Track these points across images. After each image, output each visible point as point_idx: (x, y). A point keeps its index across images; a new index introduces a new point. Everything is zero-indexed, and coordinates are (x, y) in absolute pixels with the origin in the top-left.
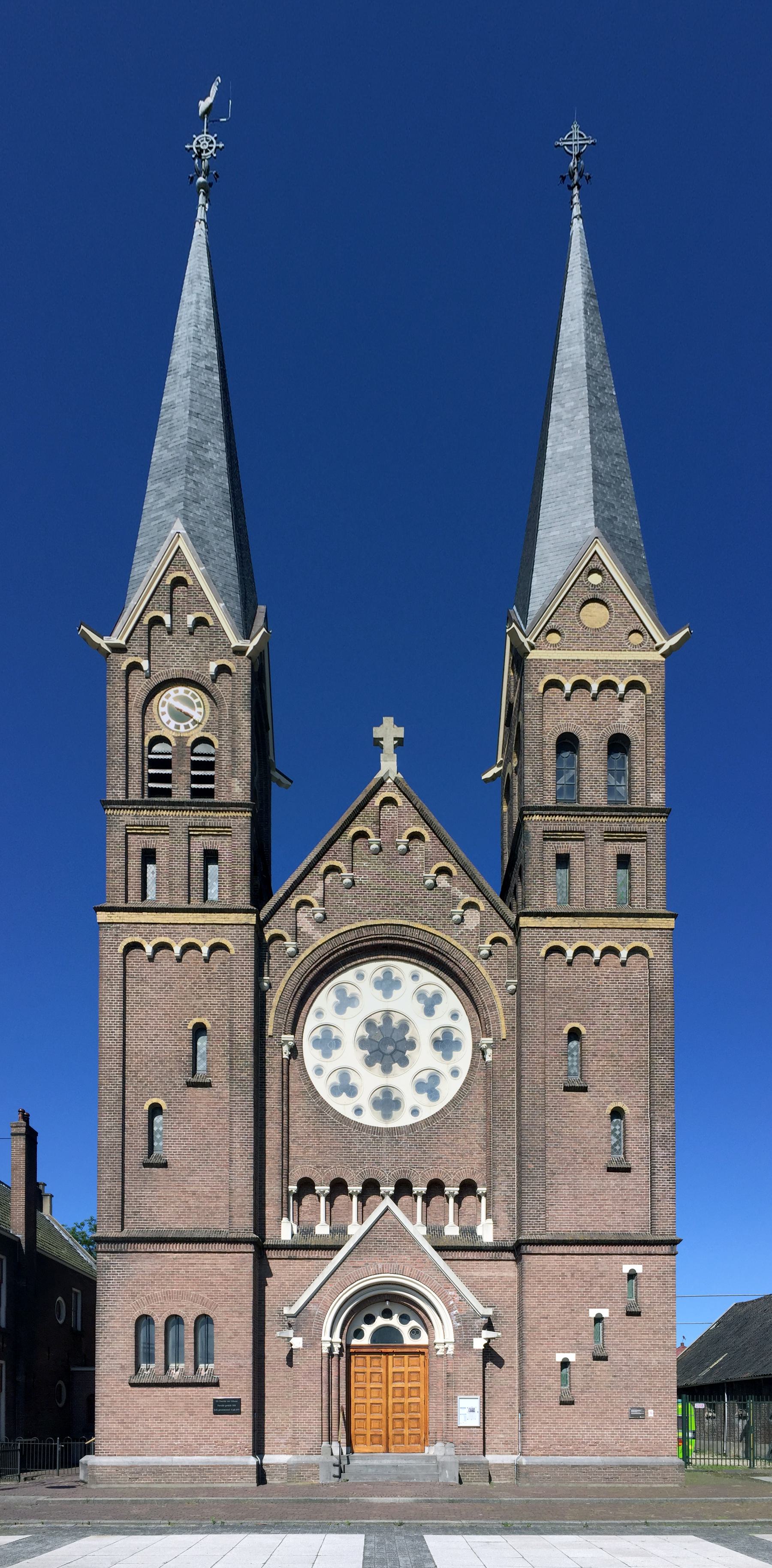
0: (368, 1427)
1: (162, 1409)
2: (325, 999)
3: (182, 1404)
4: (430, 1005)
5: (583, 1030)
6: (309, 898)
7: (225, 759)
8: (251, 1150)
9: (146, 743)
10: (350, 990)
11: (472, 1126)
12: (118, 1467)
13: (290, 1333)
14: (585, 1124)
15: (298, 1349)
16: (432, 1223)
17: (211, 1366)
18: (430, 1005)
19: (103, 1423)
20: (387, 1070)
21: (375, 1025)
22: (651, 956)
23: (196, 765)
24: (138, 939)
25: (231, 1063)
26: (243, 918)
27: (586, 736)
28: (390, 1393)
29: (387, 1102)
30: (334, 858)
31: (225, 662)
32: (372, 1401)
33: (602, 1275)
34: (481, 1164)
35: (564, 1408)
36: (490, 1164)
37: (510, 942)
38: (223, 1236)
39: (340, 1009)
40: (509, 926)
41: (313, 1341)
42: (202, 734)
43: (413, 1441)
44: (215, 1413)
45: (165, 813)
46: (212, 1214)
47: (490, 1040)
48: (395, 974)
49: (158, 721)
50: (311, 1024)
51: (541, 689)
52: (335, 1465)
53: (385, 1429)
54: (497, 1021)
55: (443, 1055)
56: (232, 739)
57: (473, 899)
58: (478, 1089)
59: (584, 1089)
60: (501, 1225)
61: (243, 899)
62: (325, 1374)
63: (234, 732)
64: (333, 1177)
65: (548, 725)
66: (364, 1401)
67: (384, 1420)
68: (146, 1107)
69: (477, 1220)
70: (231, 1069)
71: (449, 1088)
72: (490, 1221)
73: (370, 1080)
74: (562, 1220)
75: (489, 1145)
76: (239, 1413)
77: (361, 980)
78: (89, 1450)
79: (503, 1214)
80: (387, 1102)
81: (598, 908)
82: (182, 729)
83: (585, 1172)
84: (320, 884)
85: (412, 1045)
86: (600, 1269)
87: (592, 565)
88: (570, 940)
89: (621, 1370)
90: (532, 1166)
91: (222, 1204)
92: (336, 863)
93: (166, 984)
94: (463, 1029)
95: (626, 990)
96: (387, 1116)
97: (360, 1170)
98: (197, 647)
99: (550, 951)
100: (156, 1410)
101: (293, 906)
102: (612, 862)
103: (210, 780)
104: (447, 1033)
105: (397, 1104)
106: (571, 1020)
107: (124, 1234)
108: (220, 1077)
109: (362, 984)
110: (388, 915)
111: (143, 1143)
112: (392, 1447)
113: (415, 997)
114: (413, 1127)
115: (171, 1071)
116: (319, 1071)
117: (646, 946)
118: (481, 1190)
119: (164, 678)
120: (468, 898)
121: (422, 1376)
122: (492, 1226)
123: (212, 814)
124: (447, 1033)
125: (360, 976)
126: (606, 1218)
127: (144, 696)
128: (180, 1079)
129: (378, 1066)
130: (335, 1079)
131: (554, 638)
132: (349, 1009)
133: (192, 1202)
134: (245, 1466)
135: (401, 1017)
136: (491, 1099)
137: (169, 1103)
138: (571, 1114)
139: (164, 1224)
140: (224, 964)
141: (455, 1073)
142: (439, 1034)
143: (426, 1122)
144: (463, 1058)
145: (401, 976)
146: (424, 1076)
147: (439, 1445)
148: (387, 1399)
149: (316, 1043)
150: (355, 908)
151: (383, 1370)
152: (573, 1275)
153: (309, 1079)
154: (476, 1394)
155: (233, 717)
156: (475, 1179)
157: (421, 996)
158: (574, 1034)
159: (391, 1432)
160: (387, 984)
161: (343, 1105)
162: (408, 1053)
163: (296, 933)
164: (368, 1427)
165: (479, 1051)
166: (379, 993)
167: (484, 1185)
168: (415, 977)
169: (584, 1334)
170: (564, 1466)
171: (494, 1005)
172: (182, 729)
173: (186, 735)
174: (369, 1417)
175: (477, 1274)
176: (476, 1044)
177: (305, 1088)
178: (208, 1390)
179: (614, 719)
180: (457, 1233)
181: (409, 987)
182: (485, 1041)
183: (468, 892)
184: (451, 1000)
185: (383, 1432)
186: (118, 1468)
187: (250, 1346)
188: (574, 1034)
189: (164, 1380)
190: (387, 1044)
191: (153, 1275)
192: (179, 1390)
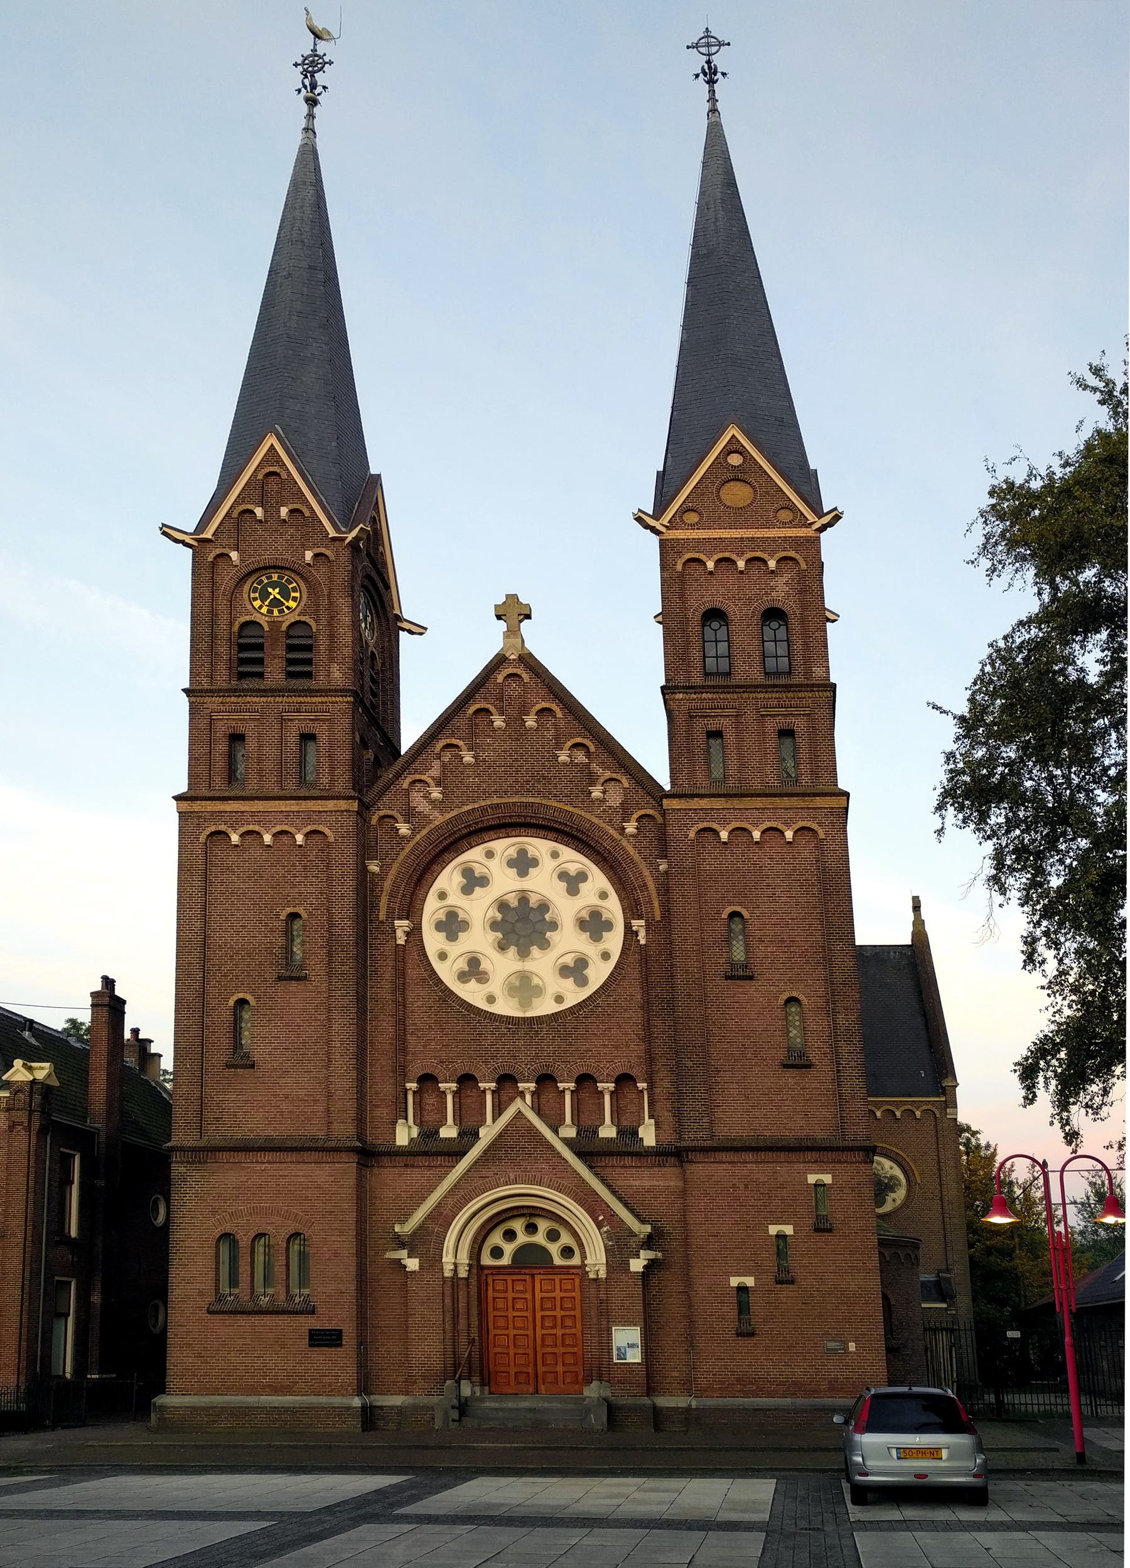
0: (512, 1363)
1: (248, 1341)
2: (449, 879)
3: (271, 1336)
4: (573, 883)
6: (423, 777)
7: (323, 643)
8: (353, 1048)
9: (236, 628)
12: (193, 1407)
13: (403, 1254)
14: (753, 1016)
15: (414, 1272)
16: (586, 1121)
17: (306, 1291)
18: (573, 883)
19: (178, 1358)
20: (524, 954)
22: (822, 836)
23: (291, 648)
24: (222, 828)
25: (329, 954)
26: (343, 805)
27: (733, 610)
28: (539, 1323)
29: (524, 987)
30: (452, 735)
31: (323, 550)
32: (516, 1332)
33: (782, 1187)
35: (742, 1341)
36: (650, 1059)
38: (320, 1144)
39: (467, 890)
41: (432, 1261)
42: (298, 618)
43: (568, 1380)
44: (311, 1345)
45: (254, 699)
46: (309, 1119)
47: (642, 922)
49: (249, 607)
50: (432, 909)
51: (679, 567)
52: (453, 1407)
53: (532, 1365)
54: (650, 902)
56: (330, 624)
57: (614, 776)
58: (634, 973)
60: (665, 1127)
61: (343, 784)
62: (448, 1301)
63: (332, 618)
65: (693, 602)
66: (506, 1332)
67: (532, 1355)
68: (231, 1003)
69: (641, 1121)
70: (330, 962)
71: (599, 973)
72: (653, 1121)
74: (734, 1123)
75: (648, 1037)
76: (340, 1345)
77: (493, 858)
78: (162, 1389)
80: (524, 987)
81: (756, 785)
82: (276, 613)
83: (756, 1069)
84: (436, 764)
85: (554, 926)
86: (781, 1179)
87: (730, 447)
88: (724, 822)
89: (812, 1296)
91: (321, 1108)
92: (454, 741)
93: (255, 873)
94: (613, 908)
95: (795, 870)
97: (492, 1064)
98: (292, 536)
100: (240, 1342)
101: (405, 785)
102: (772, 741)
103: (309, 662)
104: (595, 914)
106: (730, 903)
107: (202, 1143)
108: (316, 968)
111: (226, 1041)
112: (542, 1388)
113: (555, 876)
114: (555, 1016)
115: (261, 963)
116: (443, 956)
117: (815, 826)
119: (256, 566)
120: (608, 774)
121: (578, 1301)
122: (653, 1128)
123: (308, 699)
124: (595, 914)
125: (490, 854)
126: (785, 1121)
127: (232, 583)
128: (270, 974)
129: (513, 950)
130: (462, 965)
131: (692, 518)
132: (477, 889)
133: (284, 1106)
134: (349, 1408)
135: (539, 897)
136: (646, 984)
137: (258, 999)
138: (737, 1005)
139: (251, 1131)
140: (322, 851)
141: (606, 956)
143: (571, 1010)
144: (614, 942)
145: (538, 854)
147: (595, 1384)
148: (535, 1329)
149: (440, 926)
150: (479, 786)
151: (528, 1296)
152: (746, 1186)
153: (430, 965)
154: (635, 1325)
155: (331, 603)
156: (634, 1073)
157: (563, 876)
159: (541, 1369)
160: (523, 864)
161: (472, 993)
162: (548, 934)
163: (409, 814)
164: (512, 1363)
165: (630, 933)
166: (513, 872)
167: (645, 1081)
168: (555, 855)
169: (765, 1255)
170: (744, 1409)
171: (645, 885)
172: (276, 613)
173: (280, 619)
174: (512, 1352)
175: (637, 1183)
176: (628, 927)
177: (425, 975)
178: (302, 1319)
179: (766, 593)
180: (614, 1135)
181: (548, 865)
182: (638, 924)
183: (608, 768)
184: (598, 880)
185: (530, 1370)
186: (194, 1409)
187: (353, 1269)
189: (250, 1306)
190: (523, 924)
191: (237, 1188)
192: (268, 1320)
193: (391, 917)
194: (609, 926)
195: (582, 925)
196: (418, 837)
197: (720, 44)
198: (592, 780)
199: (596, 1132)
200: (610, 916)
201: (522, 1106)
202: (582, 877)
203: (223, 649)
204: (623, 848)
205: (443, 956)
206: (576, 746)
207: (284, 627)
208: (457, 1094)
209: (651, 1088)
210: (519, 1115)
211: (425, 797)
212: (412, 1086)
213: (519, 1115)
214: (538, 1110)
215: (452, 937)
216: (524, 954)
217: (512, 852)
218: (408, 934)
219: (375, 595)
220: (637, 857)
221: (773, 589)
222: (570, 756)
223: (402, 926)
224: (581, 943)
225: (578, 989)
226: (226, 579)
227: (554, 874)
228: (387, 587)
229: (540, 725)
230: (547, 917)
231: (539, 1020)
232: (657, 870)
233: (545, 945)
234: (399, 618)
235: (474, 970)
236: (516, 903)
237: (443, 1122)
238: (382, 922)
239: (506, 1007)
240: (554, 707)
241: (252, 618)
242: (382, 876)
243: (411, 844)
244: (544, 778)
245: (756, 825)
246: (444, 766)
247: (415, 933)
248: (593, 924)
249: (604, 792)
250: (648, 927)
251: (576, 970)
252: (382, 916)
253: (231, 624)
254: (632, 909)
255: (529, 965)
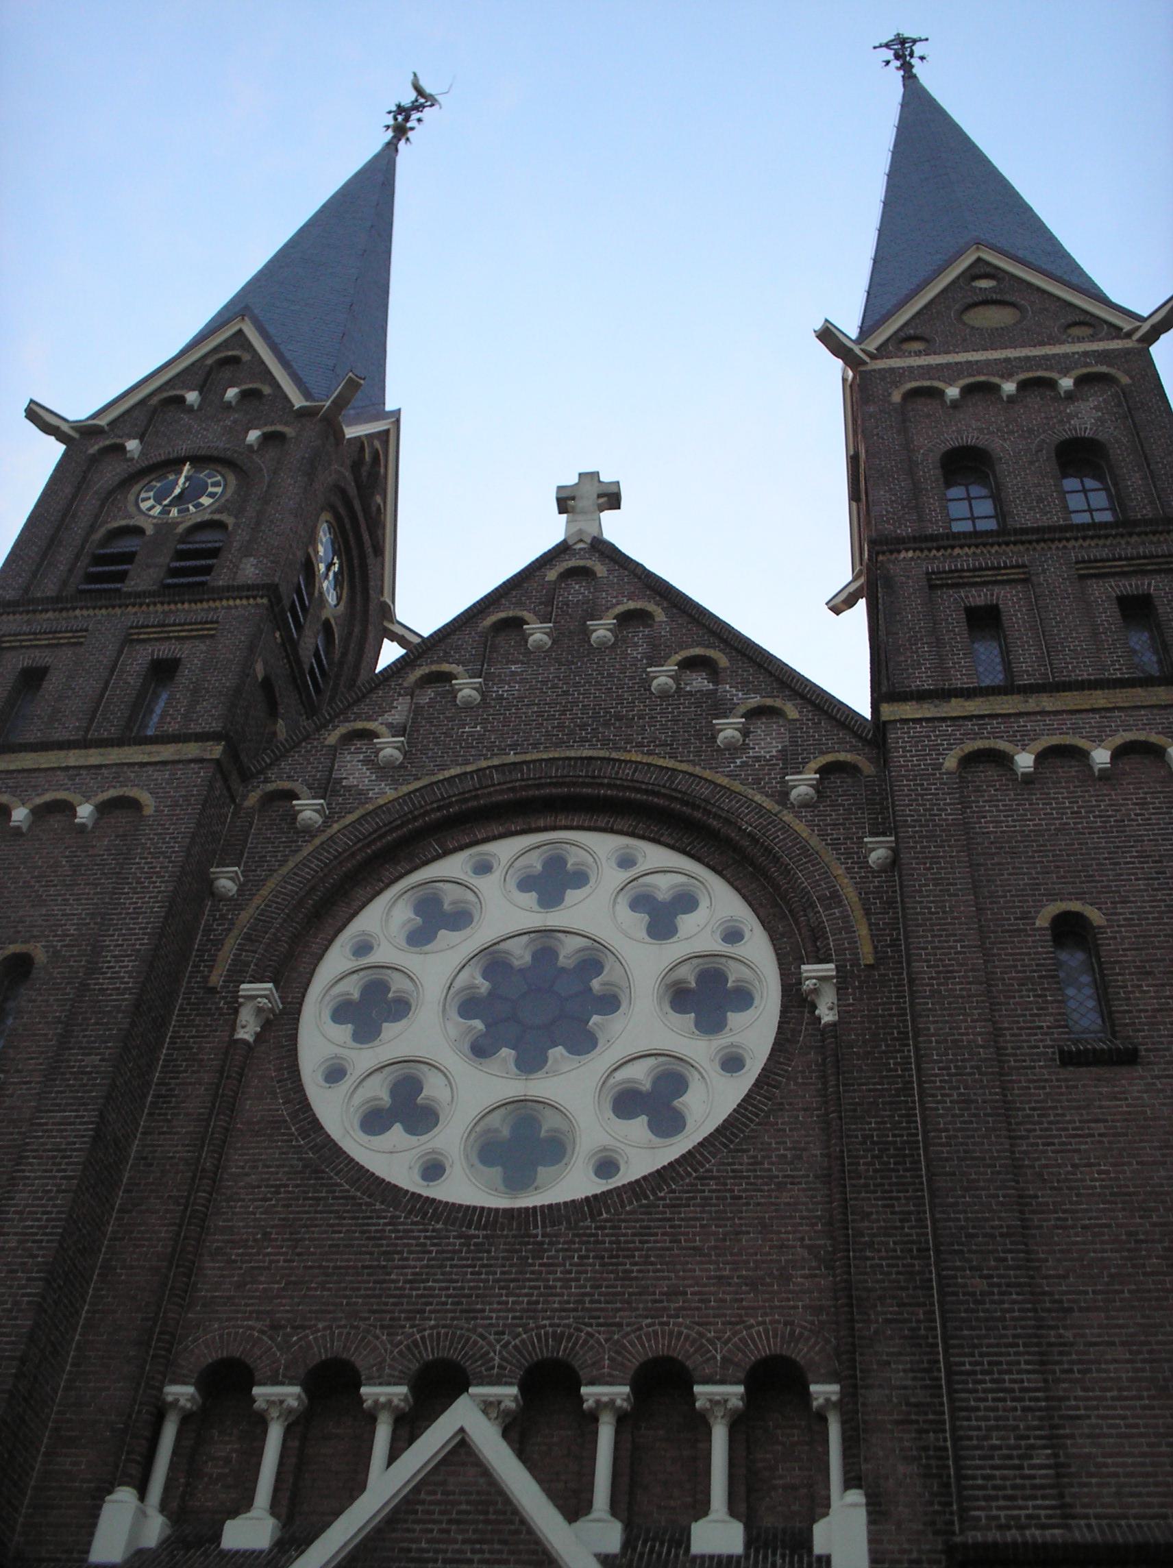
2: (384, 918)
4: (661, 918)
5: (1095, 916)
6: (371, 725)
10: (451, 894)
11: (785, 1198)
18: (661, 918)
21: (510, 966)
34: (866, 1387)
37: (868, 768)
39: (420, 937)
40: (860, 737)
47: (829, 968)
48: (574, 858)
50: (335, 967)
55: (698, 1025)
57: (769, 702)
59: (1129, 1057)
64: (319, 1354)
69: (819, 1506)
71: (711, 1102)
72: (856, 1497)
73: (473, 1091)
79: (901, 1469)
80: (523, 1140)
85: (610, 1003)
90: (980, 1285)
94: (757, 955)
96: (518, 1179)
99: (971, 760)
101: (332, 738)
105: (555, 1149)
106: (1053, 896)
109: (488, 886)
110: (557, 745)
114: (593, 1204)
118: (823, 1391)
120: (755, 701)
125: (484, 868)
130: (379, 1090)
135: (580, 942)
141: (732, 1063)
142: (688, 974)
143: (635, 1188)
144: (756, 1030)
146: (640, 1074)
149: (342, 1012)
153: (299, 1088)
156: (801, 1353)
158: (1070, 930)
160: (553, 882)
161: (391, 1158)
165: (796, 1001)
166: (530, 899)
168: (626, 862)
188: (1070, 930)
190: (538, 1003)
193: (238, 974)
194: (743, 998)
195: (680, 997)
196: (336, 827)
197: (914, 41)
198: (721, 708)
199: (683, 1539)
200: (746, 973)
201: (469, 1418)
202: (686, 902)
203: (64, 557)
204: (786, 828)
205: (335, 1074)
206: (690, 664)
207: (180, 529)
208: (298, 1427)
209: (849, 1406)
210: (461, 1447)
211: (366, 762)
212: (182, 1393)
213: (461, 1447)
214: (517, 1431)
215: (366, 1033)
216: (531, 1063)
217: (535, 862)
218: (267, 1025)
219: (355, 553)
220: (814, 842)
221: (1070, 417)
222: (676, 678)
223: (259, 992)
224: (676, 1035)
225: (657, 1141)
226: (111, 473)
227: (618, 900)
228: (379, 551)
229: (620, 640)
230: (596, 984)
231: (551, 1213)
232: (864, 864)
233: (584, 1043)
234: (387, 612)
235: (407, 1106)
236: (528, 958)
237: (243, 1504)
238: (213, 990)
239: (465, 1188)
240: (651, 607)
241: (132, 522)
242: (238, 903)
243: (317, 841)
244: (619, 718)
245: (1099, 740)
246: (417, 710)
247: (282, 1026)
248: (704, 995)
249: (746, 733)
250: (843, 982)
251: (655, 1101)
252: (217, 978)
253: (92, 528)
254: (796, 934)
255: (539, 1087)
